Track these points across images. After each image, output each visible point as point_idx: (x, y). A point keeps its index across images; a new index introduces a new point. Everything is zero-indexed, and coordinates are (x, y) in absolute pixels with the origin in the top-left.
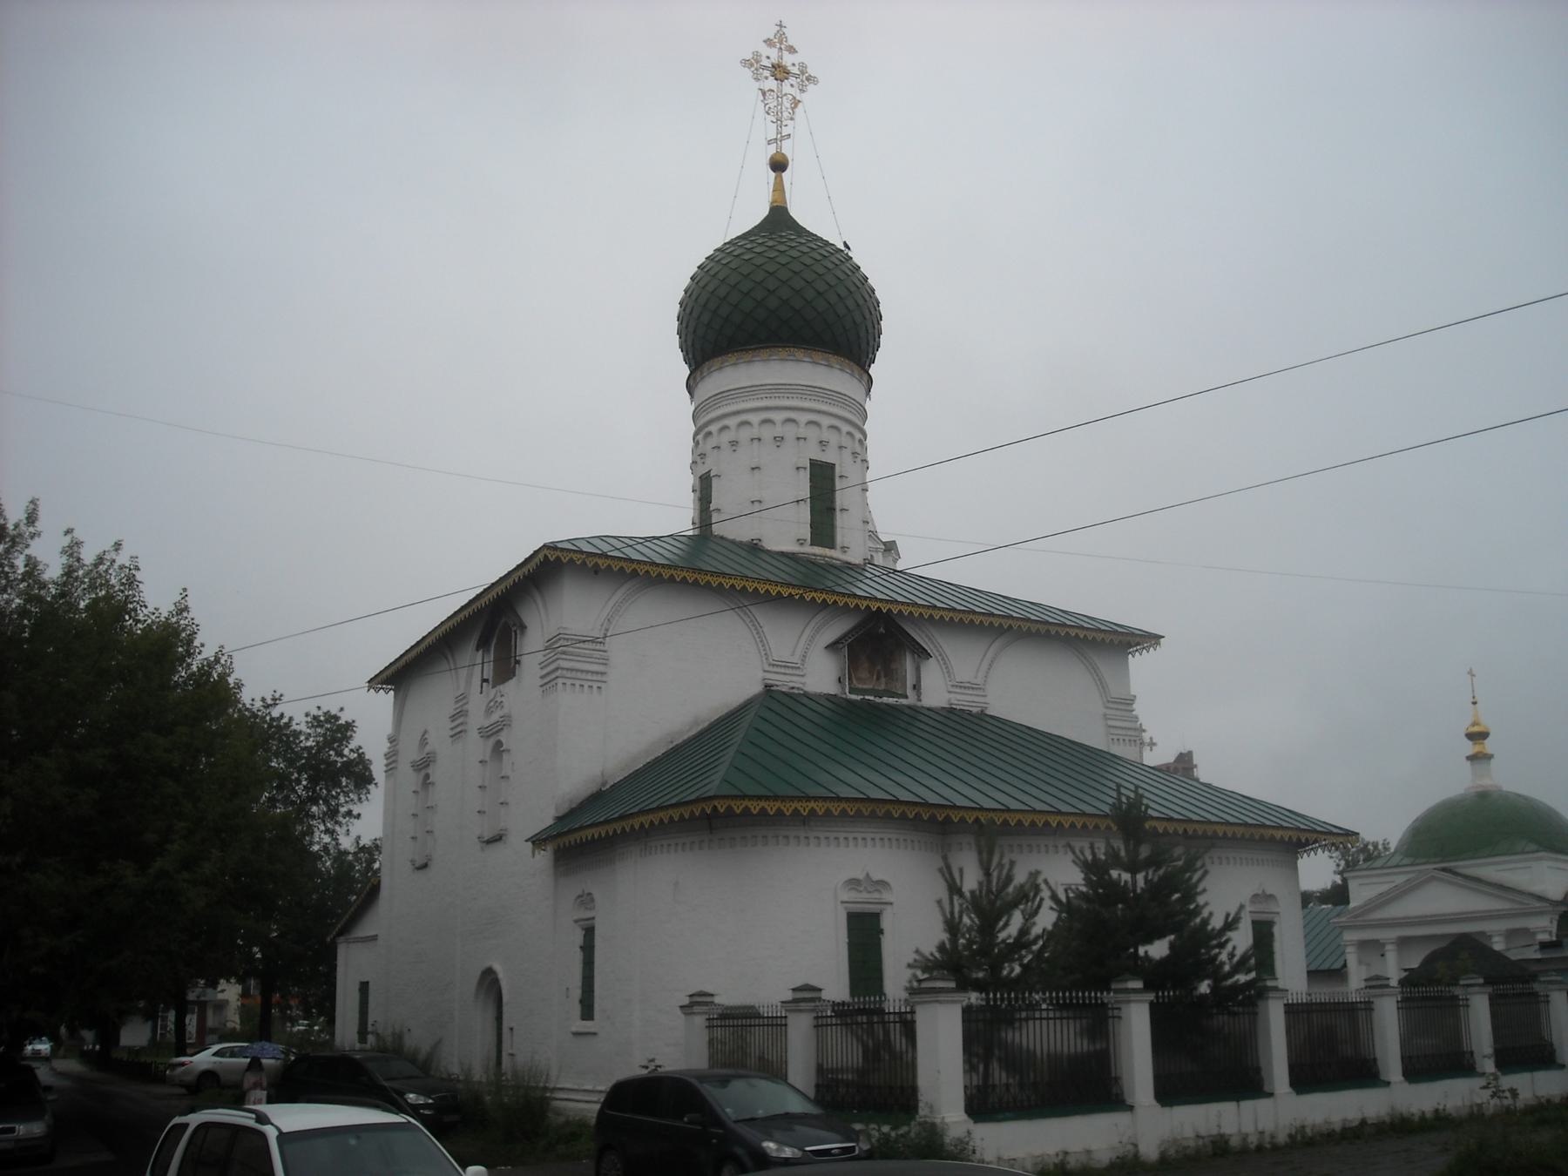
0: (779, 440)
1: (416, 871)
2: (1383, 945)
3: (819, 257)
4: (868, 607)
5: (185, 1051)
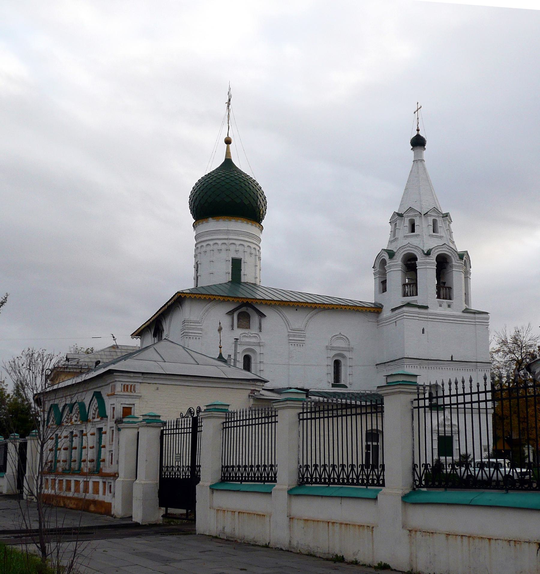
0: (220, 250)
3: (242, 181)
5: (448, 437)
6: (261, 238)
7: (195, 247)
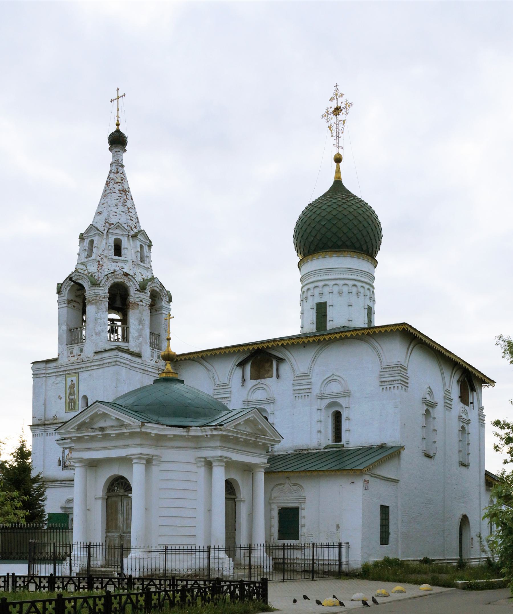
1: (424, 456)
2: (131, 460)
4: (253, 348)
6: (375, 276)
7: (301, 291)
